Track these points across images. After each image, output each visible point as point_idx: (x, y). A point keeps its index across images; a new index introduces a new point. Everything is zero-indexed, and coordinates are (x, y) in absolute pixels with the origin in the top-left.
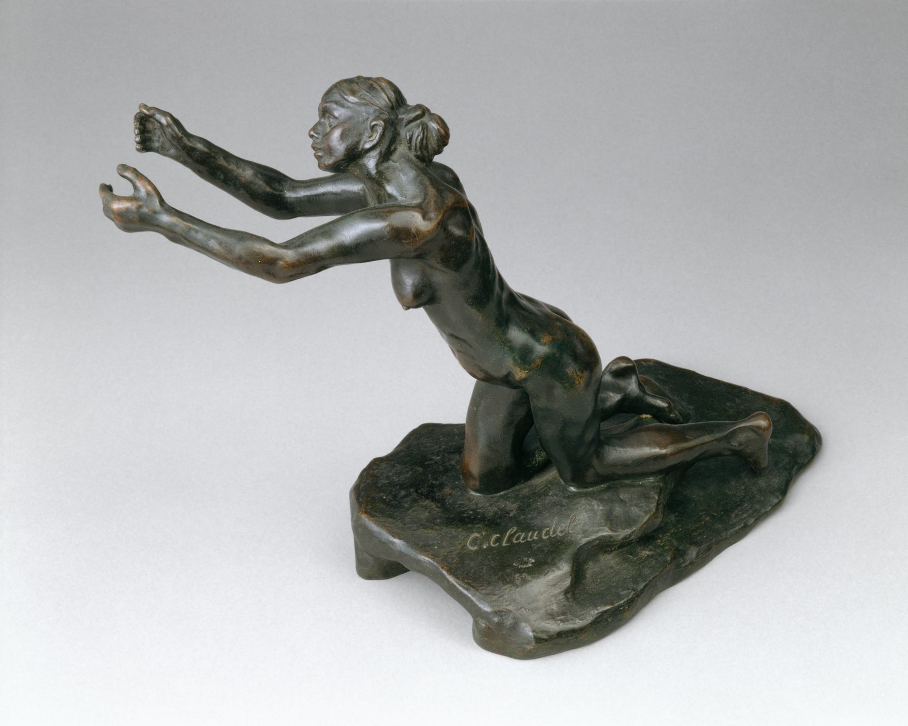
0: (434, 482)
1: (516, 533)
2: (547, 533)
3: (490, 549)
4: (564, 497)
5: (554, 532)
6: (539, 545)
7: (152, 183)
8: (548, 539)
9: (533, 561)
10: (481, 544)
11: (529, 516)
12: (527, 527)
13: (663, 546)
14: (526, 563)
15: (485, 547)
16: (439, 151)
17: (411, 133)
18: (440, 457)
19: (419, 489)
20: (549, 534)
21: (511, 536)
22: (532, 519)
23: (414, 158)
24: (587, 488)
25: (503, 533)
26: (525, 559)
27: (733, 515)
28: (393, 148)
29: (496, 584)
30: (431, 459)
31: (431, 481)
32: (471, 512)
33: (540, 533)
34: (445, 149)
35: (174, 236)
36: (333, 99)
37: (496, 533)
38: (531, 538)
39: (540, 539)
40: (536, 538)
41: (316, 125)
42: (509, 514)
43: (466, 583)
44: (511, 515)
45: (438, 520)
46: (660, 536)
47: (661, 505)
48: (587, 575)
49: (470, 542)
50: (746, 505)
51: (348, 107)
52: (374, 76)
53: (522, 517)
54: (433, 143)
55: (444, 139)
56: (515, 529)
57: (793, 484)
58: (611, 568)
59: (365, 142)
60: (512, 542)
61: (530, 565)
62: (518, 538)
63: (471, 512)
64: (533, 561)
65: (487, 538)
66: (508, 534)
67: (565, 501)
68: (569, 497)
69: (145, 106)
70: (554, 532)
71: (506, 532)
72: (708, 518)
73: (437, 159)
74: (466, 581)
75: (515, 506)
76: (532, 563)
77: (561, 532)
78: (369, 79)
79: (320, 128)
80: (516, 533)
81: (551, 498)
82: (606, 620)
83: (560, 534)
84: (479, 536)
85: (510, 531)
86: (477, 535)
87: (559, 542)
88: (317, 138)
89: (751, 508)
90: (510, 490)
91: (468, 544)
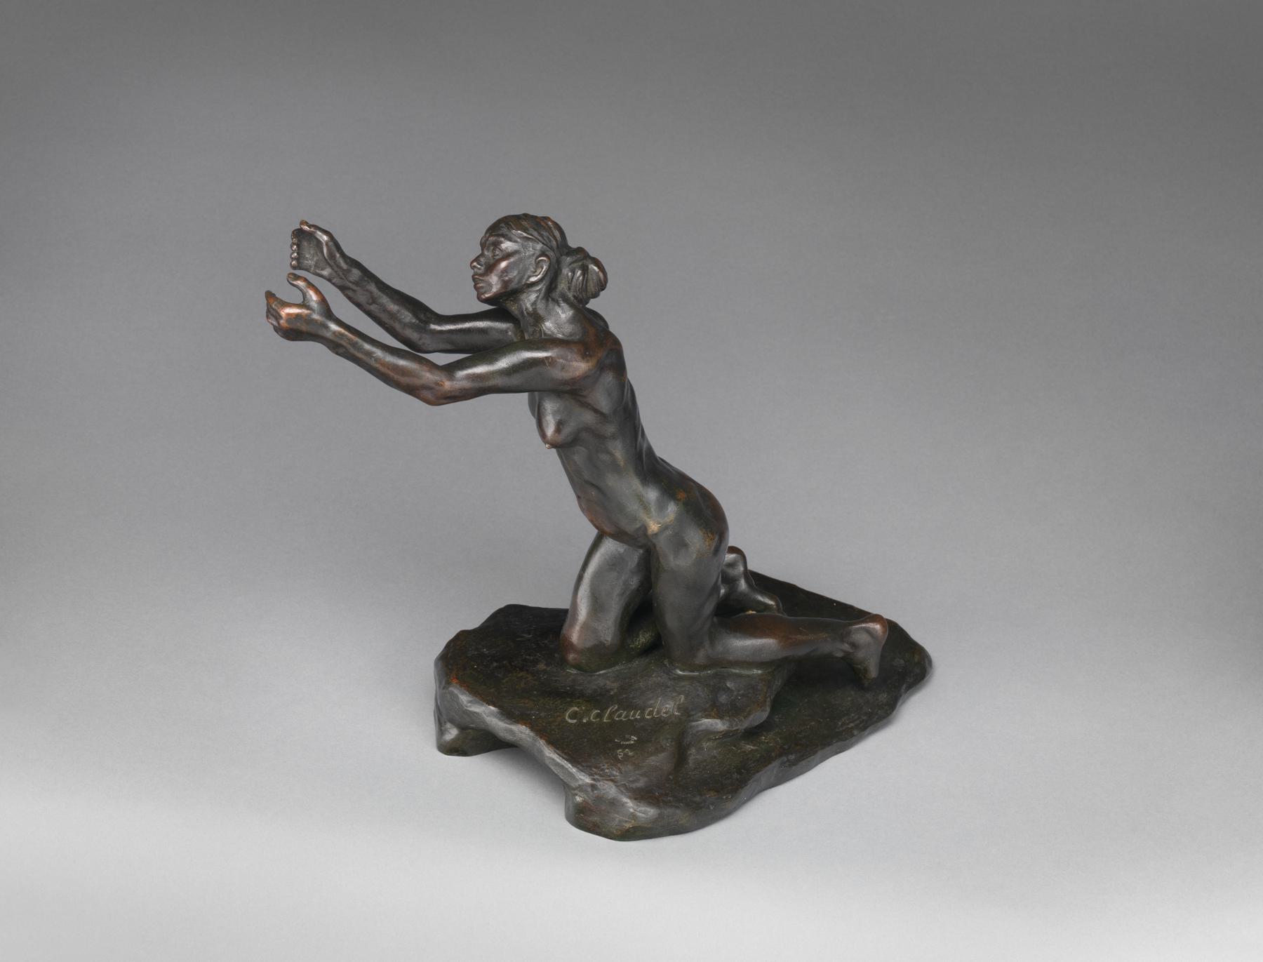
0: (528, 657)
1: (617, 710)
2: (651, 713)
3: (589, 723)
4: (670, 679)
5: (658, 712)
6: (642, 724)
7: (320, 292)
8: (651, 719)
9: (635, 738)
10: (581, 718)
11: (631, 696)
12: (629, 706)
13: (767, 743)
14: (628, 740)
15: (585, 721)
16: (595, 295)
17: (571, 275)
18: (531, 636)
19: (513, 662)
20: (652, 714)
21: (612, 713)
22: (634, 698)
23: (572, 298)
24: (693, 671)
25: (603, 710)
26: (627, 736)
27: (840, 723)
28: (553, 286)
29: (598, 757)
30: (523, 637)
31: (524, 656)
32: (568, 688)
33: (642, 713)
34: (602, 293)
35: (335, 346)
36: (500, 232)
37: (596, 709)
38: (632, 716)
39: (643, 719)
40: (639, 717)
41: (478, 257)
42: (610, 692)
43: (565, 753)
44: (612, 693)
45: (535, 692)
46: (765, 733)
47: (769, 699)
48: (689, 761)
49: (569, 715)
50: (853, 715)
51: (515, 242)
52: (540, 214)
53: (624, 696)
54: (592, 287)
55: (602, 285)
56: (616, 707)
57: (904, 702)
58: (715, 757)
59: (530, 277)
60: (613, 719)
61: (632, 742)
62: (620, 716)
63: (568, 688)
64: (635, 738)
65: (588, 712)
66: (608, 712)
67: (670, 683)
68: (674, 679)
69: (307, 224)
70: (658, 712)
71: (607, 708)
72: (813, 723)
73: (587, 306)
74: (566, 751)
75: (616, 685)
76: (635, 740)
77: (666, 713)
78: (536, 217)
79: (482, 260)
80: (617, 710)
81: (655, 679)
82: (708, 808)
83: (664, 715)
84: (577, 709)
85: (610, 708)
86: (576, 709)
87: (663, 722)
88: (479, 269)
89: (859, 718)
90: (610, 670)
91: (567, 718)
